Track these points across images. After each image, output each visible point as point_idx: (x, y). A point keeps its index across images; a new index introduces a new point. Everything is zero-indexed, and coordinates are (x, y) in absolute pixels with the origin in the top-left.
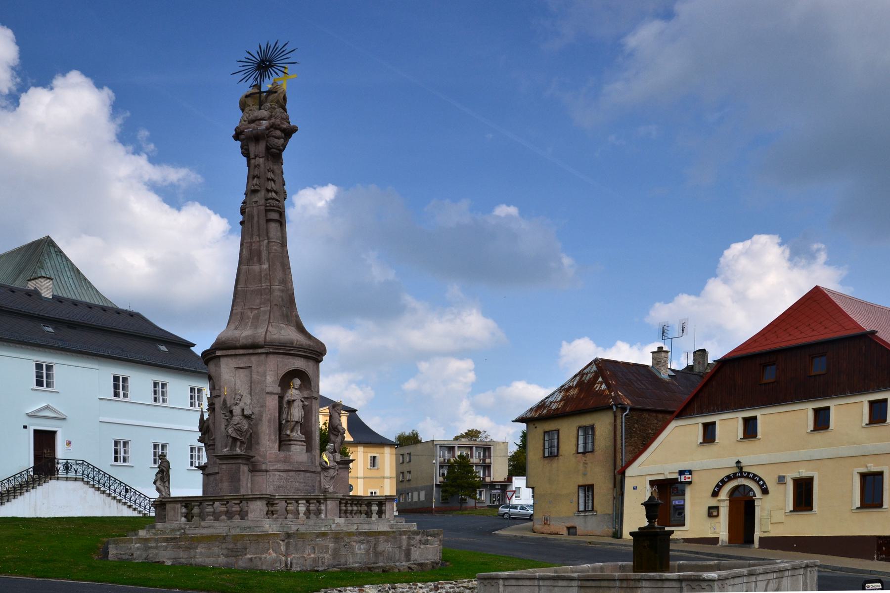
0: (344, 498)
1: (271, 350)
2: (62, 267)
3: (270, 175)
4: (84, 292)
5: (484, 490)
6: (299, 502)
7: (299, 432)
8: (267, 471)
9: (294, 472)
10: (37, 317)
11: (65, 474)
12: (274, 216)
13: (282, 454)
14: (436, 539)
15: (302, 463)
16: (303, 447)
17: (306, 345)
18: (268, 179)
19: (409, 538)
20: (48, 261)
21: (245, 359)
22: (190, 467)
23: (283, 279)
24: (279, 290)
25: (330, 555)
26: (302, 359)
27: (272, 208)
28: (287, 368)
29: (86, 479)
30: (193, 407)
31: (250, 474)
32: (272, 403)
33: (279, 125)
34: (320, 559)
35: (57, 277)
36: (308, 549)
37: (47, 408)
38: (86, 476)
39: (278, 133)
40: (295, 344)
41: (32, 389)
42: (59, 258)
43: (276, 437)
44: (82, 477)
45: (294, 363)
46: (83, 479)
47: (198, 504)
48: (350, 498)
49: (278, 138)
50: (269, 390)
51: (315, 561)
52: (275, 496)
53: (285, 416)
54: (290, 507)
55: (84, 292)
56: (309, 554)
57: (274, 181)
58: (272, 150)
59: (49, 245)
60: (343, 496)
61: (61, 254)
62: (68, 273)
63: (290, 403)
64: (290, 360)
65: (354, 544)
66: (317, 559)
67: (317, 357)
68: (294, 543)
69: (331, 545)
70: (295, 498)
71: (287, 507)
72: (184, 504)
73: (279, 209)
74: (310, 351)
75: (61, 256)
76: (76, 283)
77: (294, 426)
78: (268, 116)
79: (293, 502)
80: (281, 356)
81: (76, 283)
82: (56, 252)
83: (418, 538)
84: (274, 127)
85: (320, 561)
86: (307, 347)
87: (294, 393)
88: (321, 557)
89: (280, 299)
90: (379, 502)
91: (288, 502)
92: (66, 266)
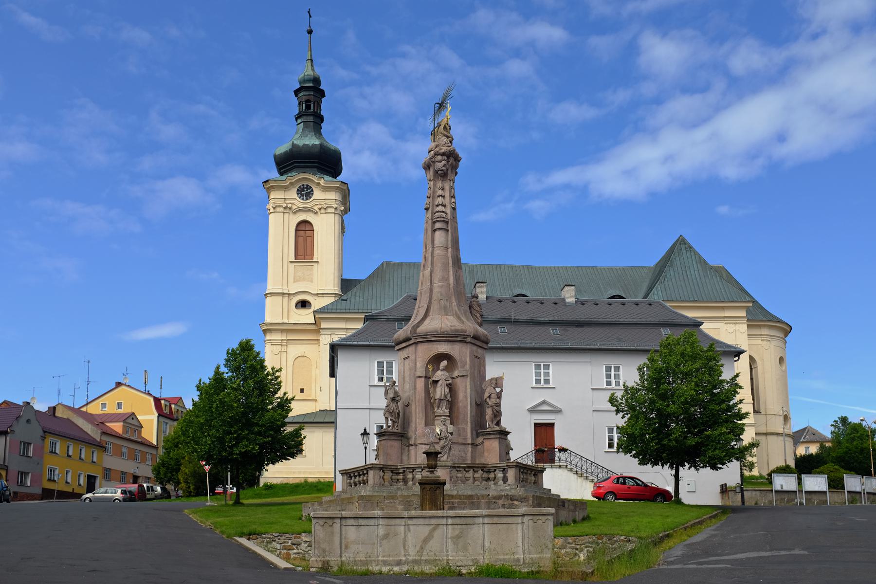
0: (454, 465)
1: (418, 340)
2: (690, 261)
3: (440, 192)
4: (708, 281)
5: (59, 442)
7: (444, 408)
8: (416, 445)
10: (548, 323)
11: (564, 462)
12: (438, 225)
13: (428, 430)
18: (438, 196)
20: (677, 258)
21: (407, 350)
22: (607, 449)
23: (443, 278)
24: (439, 286)
27: (436, 220)
28: (432, 353)
29: (569, 466)
31: (407, 448)
32: (421, 383)
33: (438, 152)
35: (684, 272)
37: (544, 402)
38: (569, 463)
39: (439, 158)
40: (439, 331)
41: (532, 387)
42: (688, 253)
43: (423, 414)
44: (565, 464)
45: (437, 349)
46: (566, 466)
48: (465, 466)
49: (441, 162)
50: (418, 374)
52: (397, 466)
53: (431, 395)
55: (708, 281)
57: (444, 197)
58: (439, 172)
59: (680, 243)
61: (691, 249)
62: (695, 266)
63: (436, 382)
67: (464, 340)
68: (363, 504)
70: (412, 467)
72: (348, 476)
73: (442, 219)
75: (691, 251)
76: (701, 273)
77: (440, 404)
78: (434, 146)
80: (427, 343)
81: (701, 273)
82: (686, 248)
84: (436, 154)
87: (440, 375)
89: (439, 295)
91: (466, 470)
92: (694, 259)
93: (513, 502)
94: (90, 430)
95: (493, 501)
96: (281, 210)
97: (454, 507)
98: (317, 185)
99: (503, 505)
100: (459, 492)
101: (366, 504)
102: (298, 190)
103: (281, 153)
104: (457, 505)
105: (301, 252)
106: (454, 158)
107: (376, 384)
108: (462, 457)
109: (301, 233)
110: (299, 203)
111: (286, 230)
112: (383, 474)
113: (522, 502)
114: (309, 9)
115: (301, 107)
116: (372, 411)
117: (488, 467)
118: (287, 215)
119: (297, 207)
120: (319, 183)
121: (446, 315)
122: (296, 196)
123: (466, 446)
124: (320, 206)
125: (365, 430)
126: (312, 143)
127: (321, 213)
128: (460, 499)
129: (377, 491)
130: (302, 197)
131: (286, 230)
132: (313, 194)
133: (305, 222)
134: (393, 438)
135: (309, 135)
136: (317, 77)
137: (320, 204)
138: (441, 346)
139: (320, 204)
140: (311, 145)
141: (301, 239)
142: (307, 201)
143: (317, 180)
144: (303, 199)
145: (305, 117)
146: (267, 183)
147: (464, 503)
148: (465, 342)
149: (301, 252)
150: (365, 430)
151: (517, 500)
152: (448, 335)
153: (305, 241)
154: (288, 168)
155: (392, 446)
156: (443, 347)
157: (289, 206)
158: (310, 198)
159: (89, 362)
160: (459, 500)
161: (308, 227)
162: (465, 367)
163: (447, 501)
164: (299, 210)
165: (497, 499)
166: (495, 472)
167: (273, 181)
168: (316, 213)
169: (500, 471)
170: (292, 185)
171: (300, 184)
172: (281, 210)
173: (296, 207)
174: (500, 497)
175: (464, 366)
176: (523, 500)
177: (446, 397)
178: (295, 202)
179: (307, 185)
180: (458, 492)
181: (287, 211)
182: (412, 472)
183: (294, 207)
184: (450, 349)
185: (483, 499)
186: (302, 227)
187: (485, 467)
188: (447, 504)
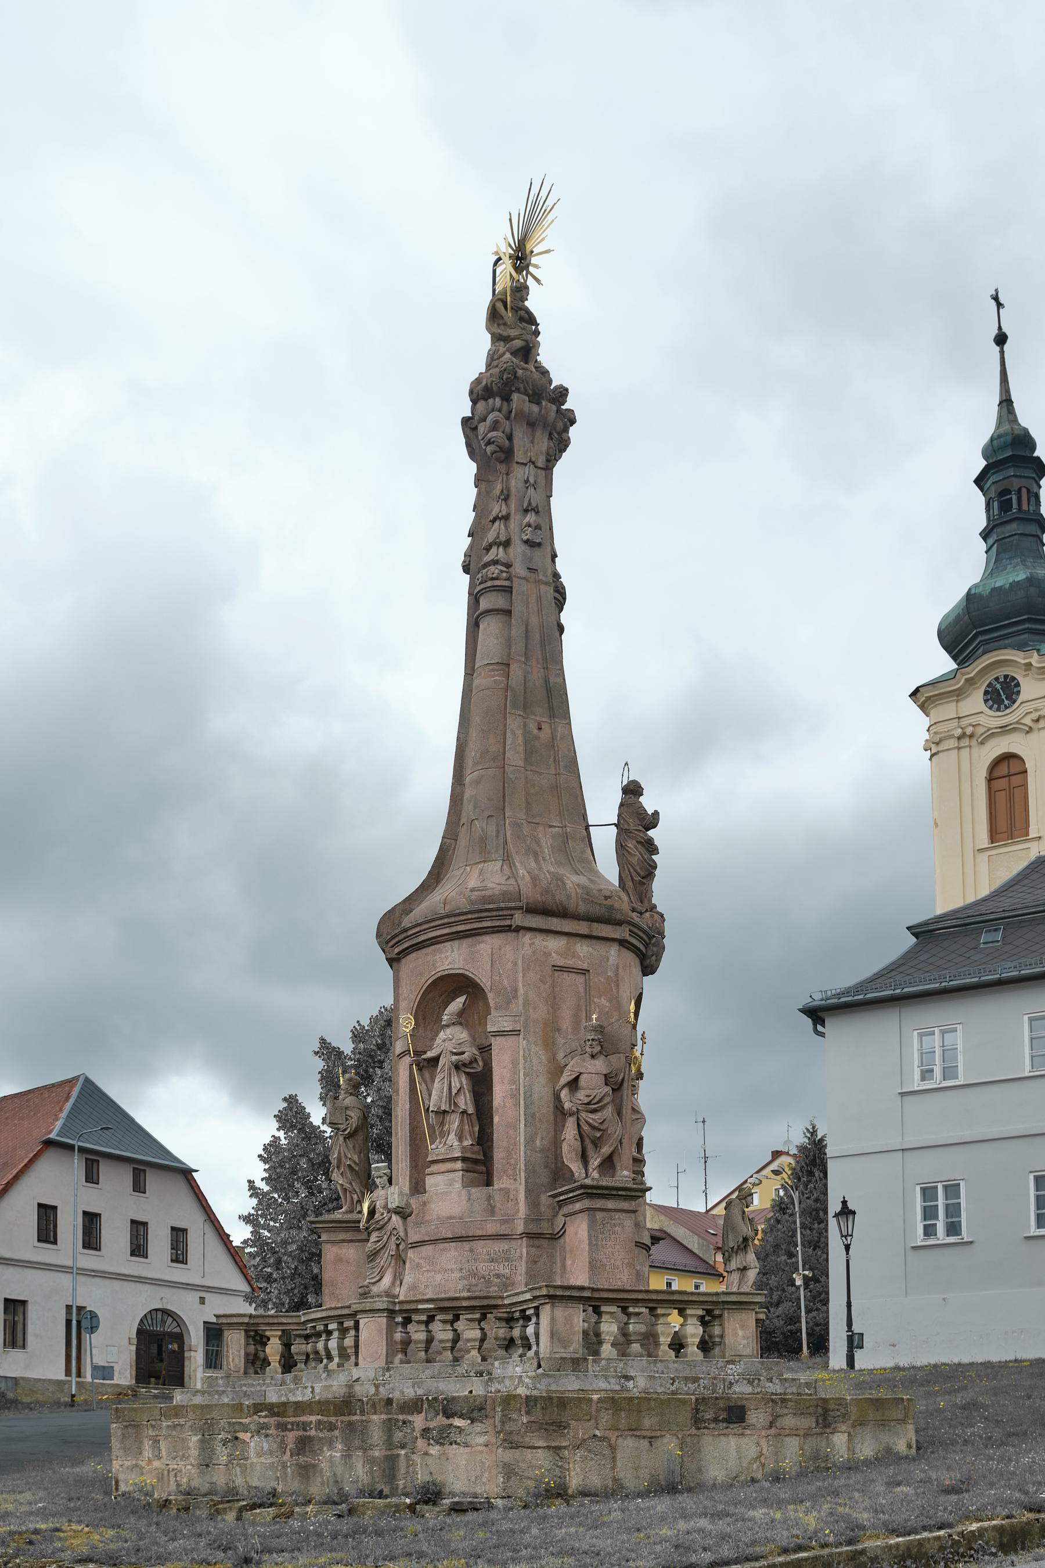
1: (397, 950)
6: (631, 1310)
9: (431, 1247)
14: (478, 1427)
15: (451, 1218)
16: (452, 1175)
17: (471, 902)
19: (389, 1426)
25: (193, 1466)
26: (456, 943)
28: (423, 981)
30: (958, 1046)
34: (172, 1474)
36: (147, 1452)
47: (478, 1316)
51: (162, 1478)
52: (502, 1298)
54: (635, 1327)
56: (150, 1461)
60: (217, 1316)
64: (429, 958)
65: (245, 1436)
66: (166, 1472)
67: (502, 923)
69: (195, 1439)
71: (626, 1324)
73: (489, 584)
74: (476, 915)
79: (643, 1310)
83: (418, 1421)
85: (172, 1479)
86: (467, 907)
88: (173, 1470)
90: (283, 1331)
93: (451, 1421)
94: (696, 1245)
95: (401, 1417)
96: (952, 743)
97: (309, 1437)
98: (1026, 670)
99: (424, 1430)
100: (381, 1389)
101: (125, 1431)
102: (986, 693)
103: (950, 623)
104: (313, 1433)
105: (1002, 824)
106: (526, 393)
107: (916, 1089)
108: (498, 1276)
109: (1002, 784)
110: (991, 719)
111: (966, 786)
112: (681, 1320)
113: (472, 1422)
114: (997, 291)
115: (991, 511)
116: (906, 1153)
117: (504, 1305)
118: (965, 752)
119: (986, 729)
120: (1030, 664)
121: (485, 862)
122: (981, 706)
123: (513, 1242)
124: (1035, 716)
125: (844, 1203)
126: (1011, 581)
127: (1040, 729)
128: (320, 1412)
129: (203, 1393)
130: (996, 706)
131: (966, 786)
132: (1018, 692)
133: (1008, 757)
134: (342, 1236)
135: (1009, 566)
136: (1023, 433)
137: (1036, 710)
138: (443, 956)
139: (1036, 710)
140: (1007, 586)
141: (1001, 797)
142: (1008, 711)
143: (1024, 659)
144: (1006, 707)
145: (999, 530)
146: (919, 695)
147: (332, 1427)
148: (509, 929)
149: (1002, 824)
150: (844, 1203)
151: (462, 1416)
152: (452, 919)
153: (1011, 799)
154: (971, 648)
155: (341, 1260)
156: (447, 957)
157: (969, 731)
158: (1014, 702)
159: (704, 1122)
160: (319, 1417)
161: (1015, 767)
162: (512, 1006)
163: (292, 1419)
164: (991, 735)
165: (409, 1414)
166: (456, 1325)
167: (930, 687)
168: (1028, 732)
169: (471, 1320)
170: (971, 685)
171: (990, 678)
172: (952, 743)
173: (984, 730)
174: (416, 1404)
175: (509, 1002)
176: (475, 1414)
177: (455, 1104)
178: (982, 720)
179: (1006, 677)
180: (377, 1387)
181: (965, 742)
182: (452, 1323)
183: (981, 730)
184: (465, 960)
185: (375, 1413)
186: (1003, 770)
187: (496, 1307)
188: (292, 1430)
